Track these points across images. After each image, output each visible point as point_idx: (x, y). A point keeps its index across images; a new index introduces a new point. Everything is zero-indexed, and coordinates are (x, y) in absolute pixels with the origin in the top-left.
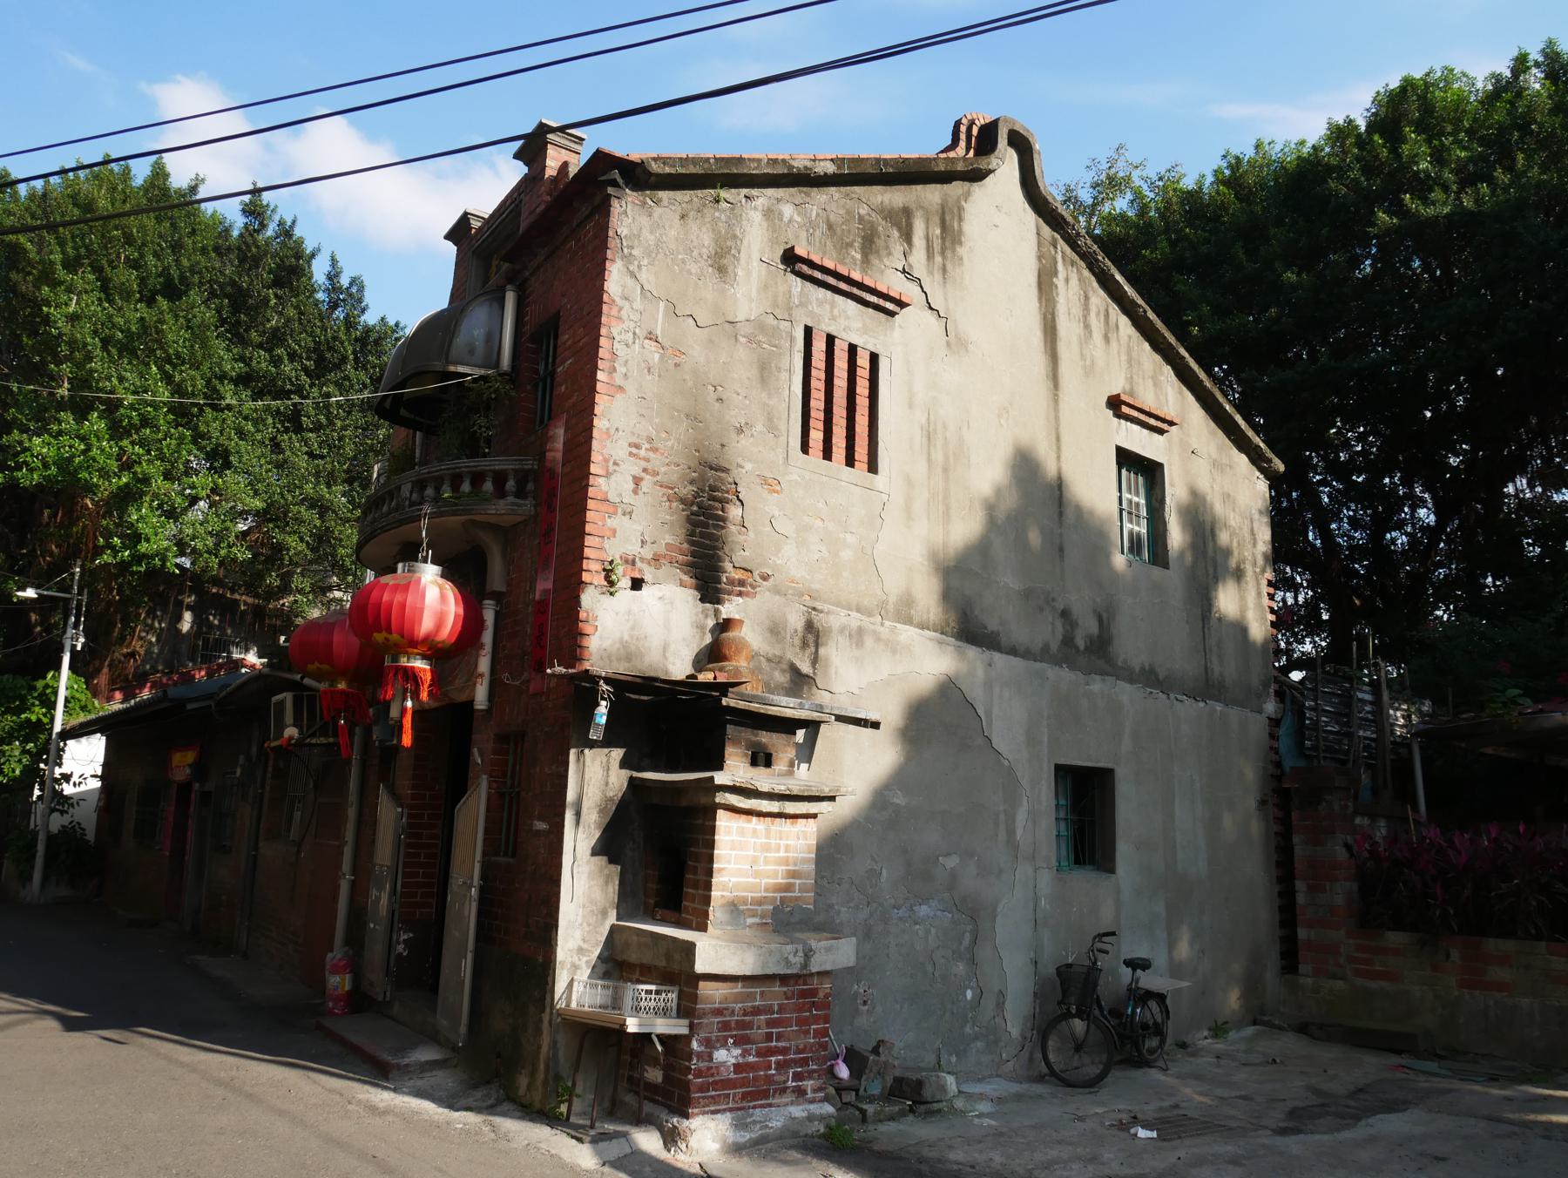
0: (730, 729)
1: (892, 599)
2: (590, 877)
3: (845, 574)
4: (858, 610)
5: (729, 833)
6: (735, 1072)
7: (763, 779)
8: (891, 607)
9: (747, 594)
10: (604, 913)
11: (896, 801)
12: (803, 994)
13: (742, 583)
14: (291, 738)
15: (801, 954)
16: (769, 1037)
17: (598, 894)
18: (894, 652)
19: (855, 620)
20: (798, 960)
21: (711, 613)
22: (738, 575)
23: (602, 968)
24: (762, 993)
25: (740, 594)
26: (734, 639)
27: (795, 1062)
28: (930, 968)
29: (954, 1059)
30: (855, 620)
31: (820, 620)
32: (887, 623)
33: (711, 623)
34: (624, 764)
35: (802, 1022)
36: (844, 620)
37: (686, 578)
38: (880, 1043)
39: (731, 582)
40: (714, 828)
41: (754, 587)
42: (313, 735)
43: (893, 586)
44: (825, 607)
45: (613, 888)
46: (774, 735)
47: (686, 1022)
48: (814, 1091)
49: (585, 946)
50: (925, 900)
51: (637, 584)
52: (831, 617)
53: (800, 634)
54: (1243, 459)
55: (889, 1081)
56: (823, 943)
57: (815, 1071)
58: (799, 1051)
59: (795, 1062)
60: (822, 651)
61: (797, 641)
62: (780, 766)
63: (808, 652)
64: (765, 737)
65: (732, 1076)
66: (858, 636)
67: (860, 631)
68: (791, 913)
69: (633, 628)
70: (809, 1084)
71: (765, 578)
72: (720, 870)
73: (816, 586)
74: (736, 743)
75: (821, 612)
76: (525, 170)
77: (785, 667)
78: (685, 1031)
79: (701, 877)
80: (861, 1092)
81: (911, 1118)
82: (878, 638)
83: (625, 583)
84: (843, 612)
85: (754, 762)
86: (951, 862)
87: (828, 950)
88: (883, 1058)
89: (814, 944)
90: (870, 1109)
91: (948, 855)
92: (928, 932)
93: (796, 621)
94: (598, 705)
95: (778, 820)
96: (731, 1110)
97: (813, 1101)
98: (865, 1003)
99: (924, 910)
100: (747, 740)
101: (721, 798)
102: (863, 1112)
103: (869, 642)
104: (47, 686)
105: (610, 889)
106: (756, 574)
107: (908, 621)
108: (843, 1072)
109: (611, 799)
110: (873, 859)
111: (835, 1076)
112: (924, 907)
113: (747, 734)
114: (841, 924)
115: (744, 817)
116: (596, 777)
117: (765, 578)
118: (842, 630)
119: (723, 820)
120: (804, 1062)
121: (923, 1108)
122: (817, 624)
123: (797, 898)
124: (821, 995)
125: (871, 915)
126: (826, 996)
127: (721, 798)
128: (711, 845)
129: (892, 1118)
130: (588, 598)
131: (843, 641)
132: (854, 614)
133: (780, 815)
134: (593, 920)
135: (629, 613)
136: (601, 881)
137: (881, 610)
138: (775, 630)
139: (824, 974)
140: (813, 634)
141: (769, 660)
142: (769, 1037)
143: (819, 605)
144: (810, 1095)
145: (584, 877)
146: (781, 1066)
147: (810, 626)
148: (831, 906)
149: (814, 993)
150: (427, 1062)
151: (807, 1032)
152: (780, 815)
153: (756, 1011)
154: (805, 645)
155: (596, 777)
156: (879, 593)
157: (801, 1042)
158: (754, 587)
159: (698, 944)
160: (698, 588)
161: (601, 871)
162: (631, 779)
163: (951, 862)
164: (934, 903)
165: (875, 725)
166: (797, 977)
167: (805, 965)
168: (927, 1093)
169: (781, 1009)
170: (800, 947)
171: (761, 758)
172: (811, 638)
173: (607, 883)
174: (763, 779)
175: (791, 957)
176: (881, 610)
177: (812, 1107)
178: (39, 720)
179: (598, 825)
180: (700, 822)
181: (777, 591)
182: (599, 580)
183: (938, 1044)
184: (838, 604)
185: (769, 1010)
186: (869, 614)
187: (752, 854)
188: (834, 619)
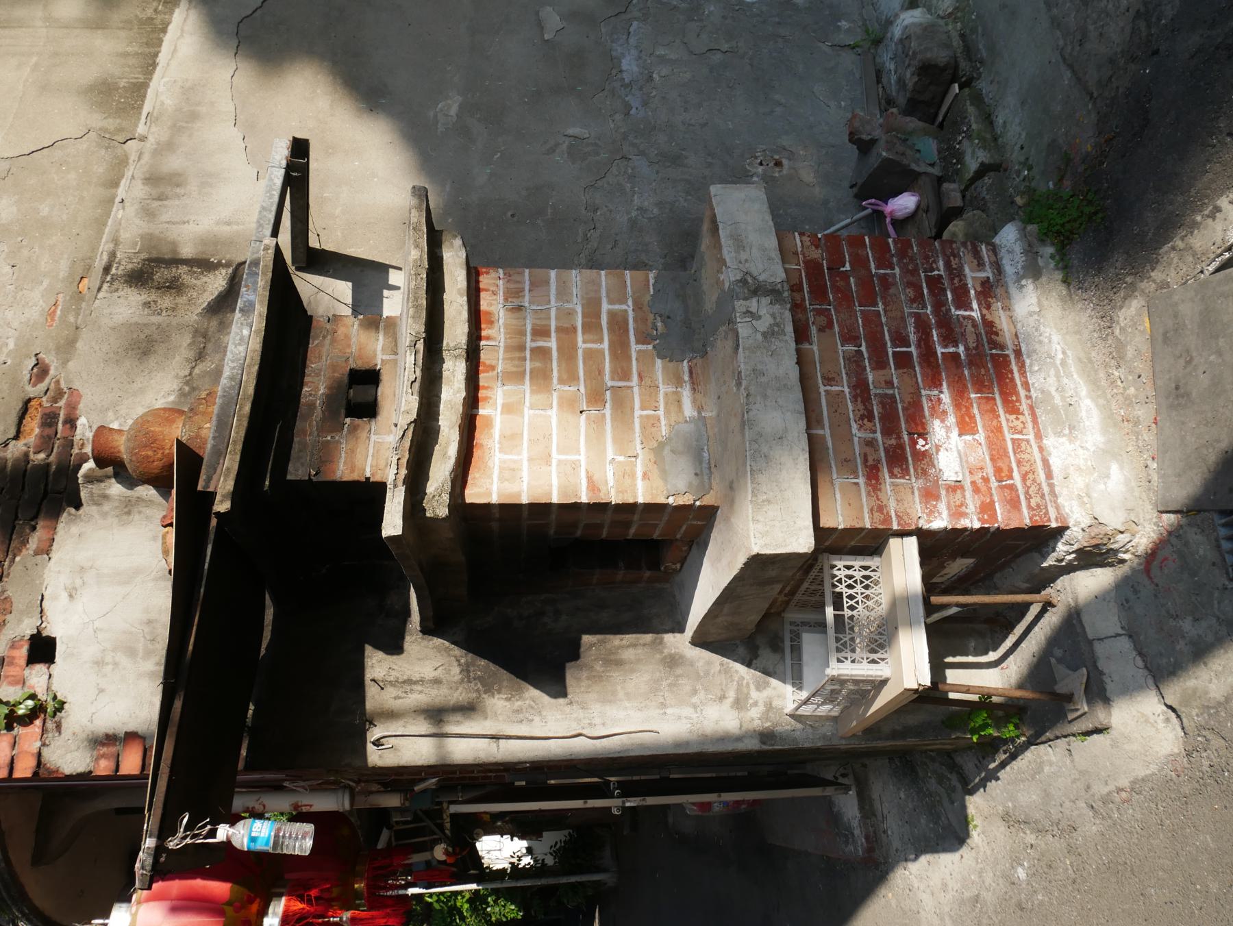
0: (297, 471)
1: (97, 120)
2: (609, 699)
3: (45, 210)
4: (115, 184)
5: (511, 472)
6: (974, 431)
7: (399, 402)
8: (111, 124)
9: (72, 407)
10: (673, 662)
11: (454, 111)
12: (819, 292)
13: (49, 420)
14: (446, 853)
15: (753, 304)
16: (903, 361)
17: (640, 680)
18: (194, 116)
19: (131, 189)
20: (764, 307)
21: (96, 488)
22: (33, 428)
23: (766, 655)
24: (829, 380)
25: (71, 422)
26: (131, 452)
27: (939, 305)
28: (717, 58)
29: (844, 24)
30: (131, 189)
31: (126, 261)
32: (141, 129)
33: (115, 489)
34: (394, 646)
35: (869, 298)
36: (131, 210)
37: (34, 541)
38: (854, 138)
39: (46, 443)
40: (503, 507)
41: (60, 394)
42: (441, 827)
43: (71, 118)
44: (105, 247)
45: (628, 645)
46: (312, 366)
47: (894, 543)
48: (981, 265)
49: (731, 695)
50: (614, 62)
51: (42, 649)
52: (125, 236)
53: (153, 296)
54: (1095, 736)
55: (913, 123)
56: (728, 254)
57: (948, 265)
58: (918, 298)
59: (939, 305)
60: (187, 252)
61: (166, 301)
62: (372, 349)
63: (187, 279)
64: (317, 386)
65: (981, 436)
66: (162, 184)
67: (153, 179)
68: (667, 318)
69: (131, 652)
70: (972, 276)
71: (41, 370)
72: (592, 486)
73: (64, 267)
74: (326, 454)
75: (113, 255)
76: (350, 284)
77: (214, 323)
78: (912, 542)
79: (608, 517)
80: (936, 171)
81: (983, 85)
82: (167, 147)
83: (37, 677)
84: (117, 213)
85: (369, 410)
86: (552, 19)
87: (740, 245)
88: (877, 133)
89: (730, 276)
90: (974, 158)
91: (540, 25)
92: (663, 60)
93: (126, 306)
94: (228, 844)
95: (484, 356)
96: (1039, 436)
97: (998, 268)
98: (778, 164)
99: (629, 66)
100: (321, 430)
101: (437, 505)
102: (983, 170)
103: (173, 163)
104: (438, 901)
105: (628, 654)
106: (32, 391)
107: (139, 90)
108: (905, 203)
109: (466, 670)
110: (552, 150)
111: (912, 217)
112: (625, 64)
113: (308, 430)
114: (660, 204)
115: (480, 437)
116: (423, 704)
117: (41, 370)
118: (148, 213)
119: (486, 488)
120: (934, 283)
121: (963, 64)
122: (135, 264)
123: (638, 307)
124: (815, 254)
125: (642, 153)
126: (816, 243)
127: (437, 505)
128: (540, 510)
129: (988, 119)
130: (69, 757)
131: (170, 212)
132: (121, 192)
133: (473, 354)
134: (686, 685)
135: (99, 663)
136: (616, 675)
137: (115, 141)
138: (143, 347)
139: (785, 253)
140: (155, 271)
141: (200, 356)
142: (903, 361)
143: (99, 264)
144: (988, 273)
145: (612, 711)
146: (949, 337)
147: (139, 278)
148: (633, 223)
149: (813, 268)
150: (861, 808)
151: (884, 280)
152: (473, 354)
153: (861, 390)
154: (174, 286)
155: (423, 704)
156: (83, 145)
157: (903, 294)
158: (60, 394)
159: (756, 550)
160: (55, 515)
161: (597, 678)
162: (427, 630)
163: (552, 19)
164: (618, 49)
165: (300, 148)
166: (797, 307)
167: (773, 293)
168: (941, 56)
169: (850, 337)
170: (740, 305)
171: (359, 394)
172: (162, 274)
173: (619, 663)
174: (399, 402)
175: (764, 324)
176: (115, 141)
177: (1009, 269)
178: (468, 901)
179: (516, 693)
180: (495, 526)
181: (67, 347)
182: (29, 736)
183: (824, 47)
184: (101, 223)
185: (855, 361)
186: (123, 162)
187: (552, 445)
188: (128, 228)
